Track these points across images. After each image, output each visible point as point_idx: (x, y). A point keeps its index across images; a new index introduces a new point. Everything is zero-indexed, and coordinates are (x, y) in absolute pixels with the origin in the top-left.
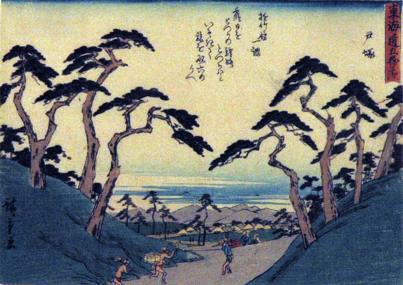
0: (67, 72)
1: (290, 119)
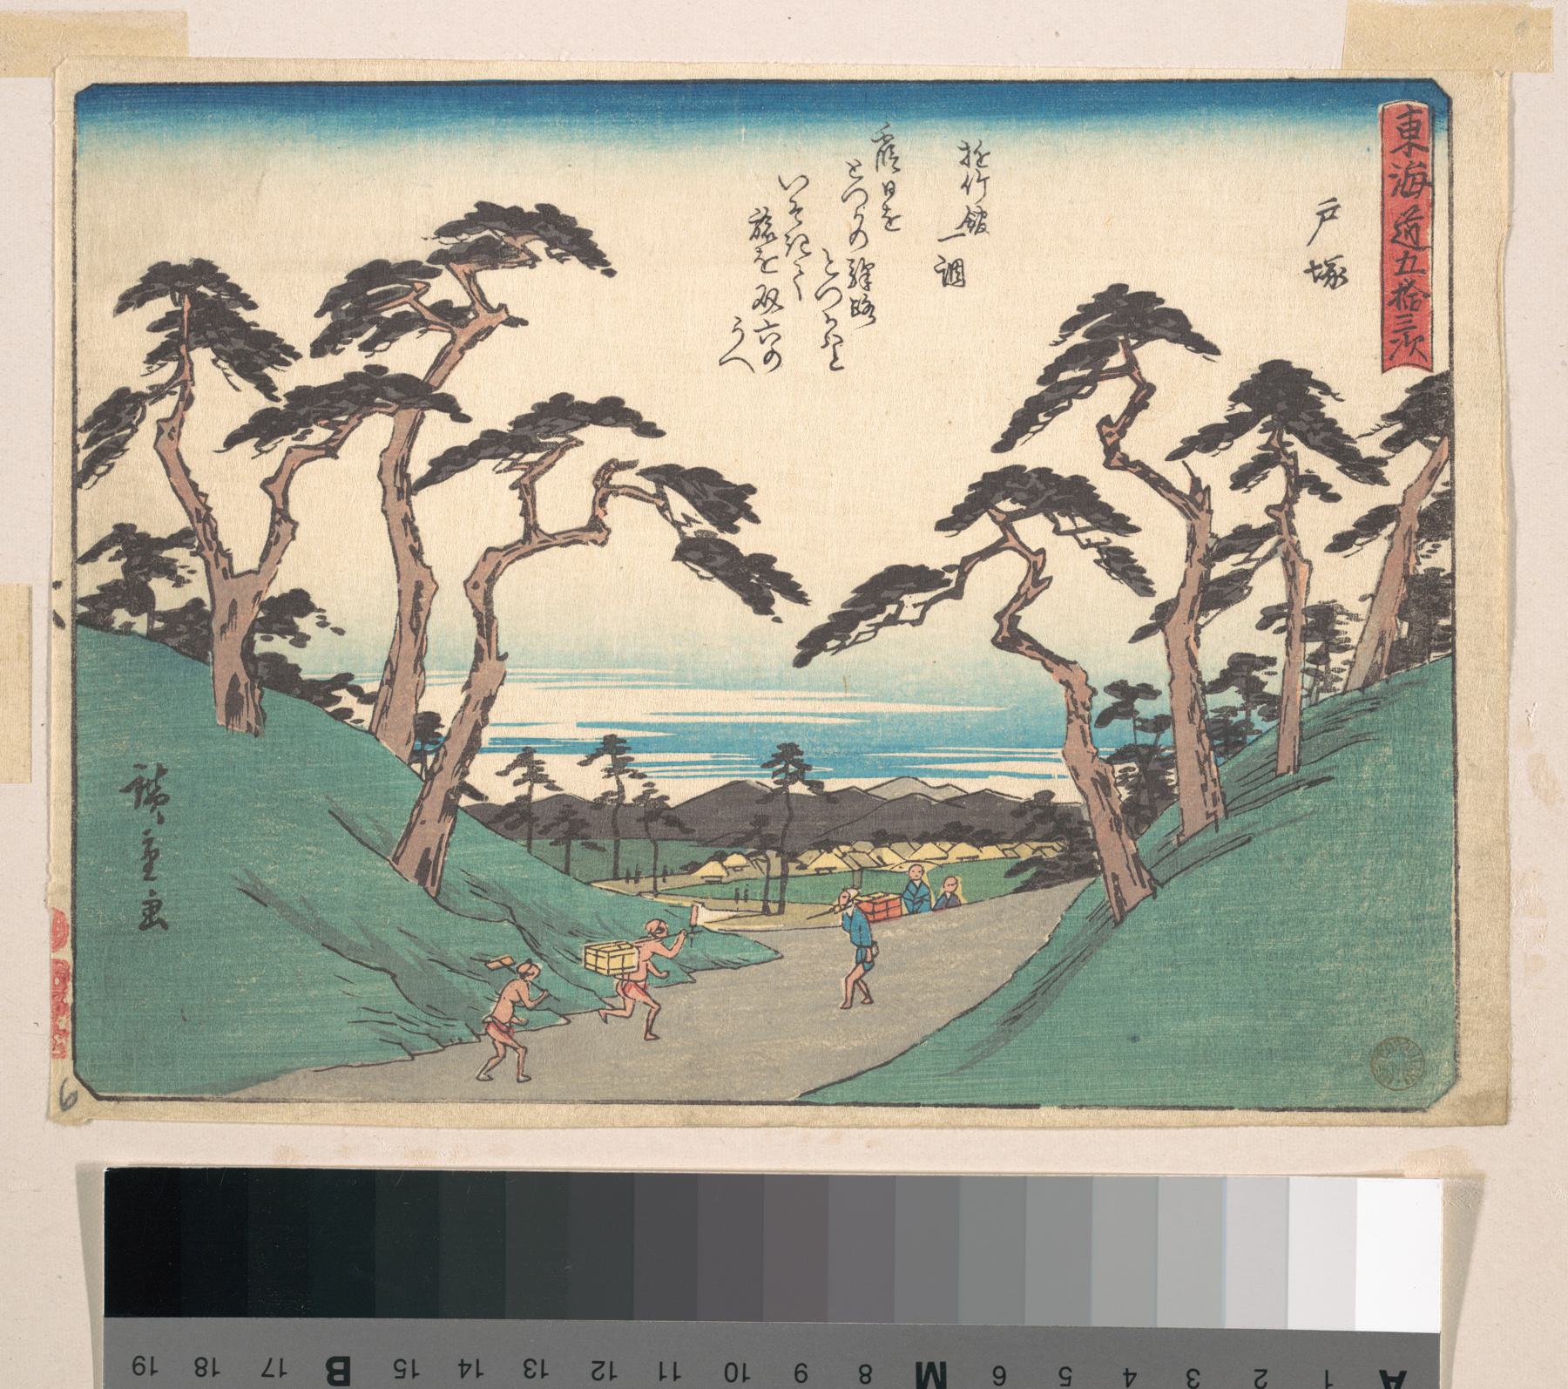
0: (324, 346)
1: (1066, 497)
